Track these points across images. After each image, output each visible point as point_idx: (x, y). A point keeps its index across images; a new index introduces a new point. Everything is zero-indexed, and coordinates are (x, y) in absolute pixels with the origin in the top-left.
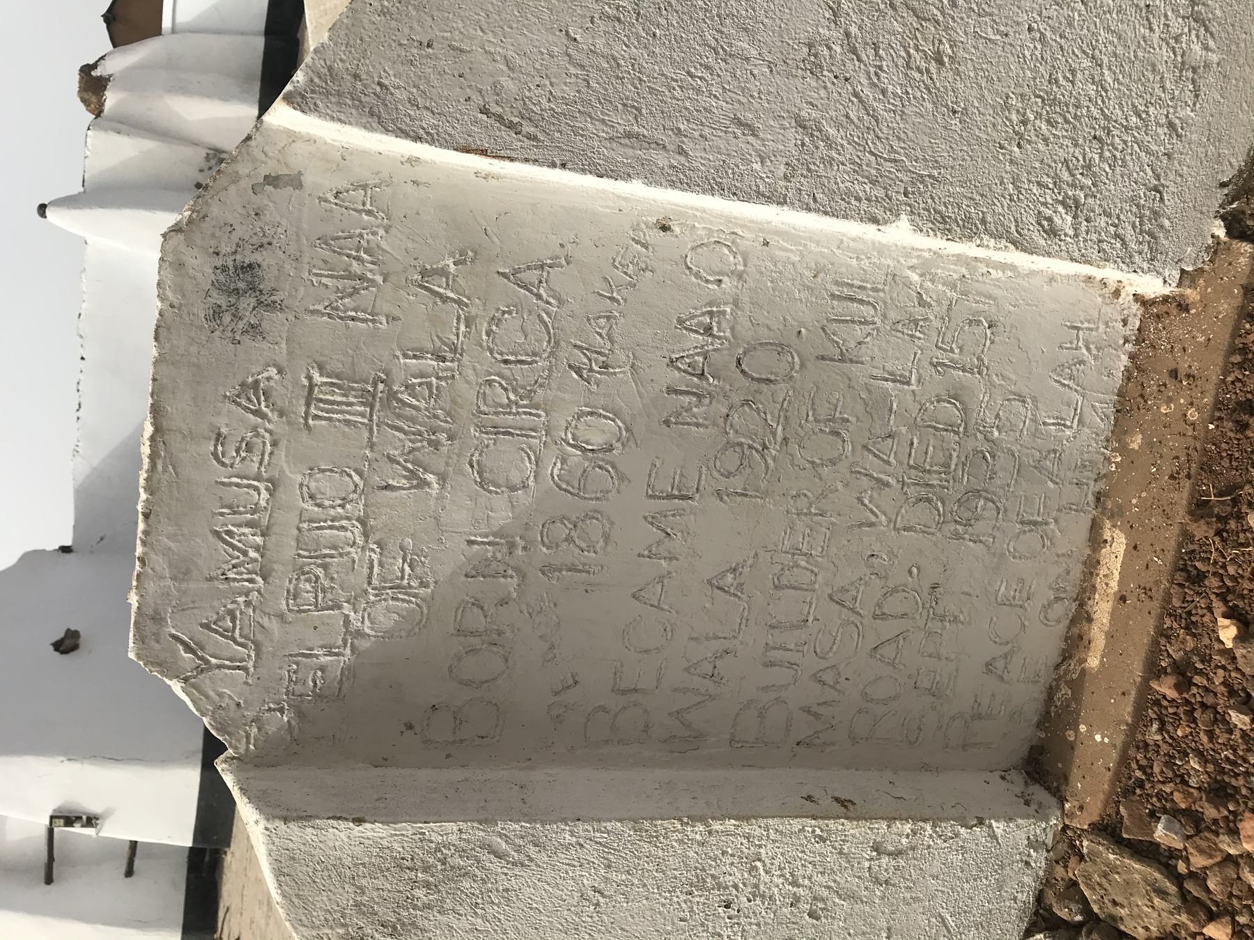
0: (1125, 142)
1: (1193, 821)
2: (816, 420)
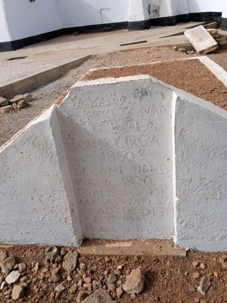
0: (199, 231)
1: (86, 269)
2: (139, 191)
